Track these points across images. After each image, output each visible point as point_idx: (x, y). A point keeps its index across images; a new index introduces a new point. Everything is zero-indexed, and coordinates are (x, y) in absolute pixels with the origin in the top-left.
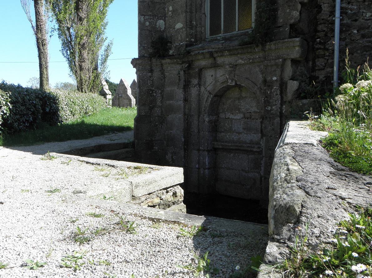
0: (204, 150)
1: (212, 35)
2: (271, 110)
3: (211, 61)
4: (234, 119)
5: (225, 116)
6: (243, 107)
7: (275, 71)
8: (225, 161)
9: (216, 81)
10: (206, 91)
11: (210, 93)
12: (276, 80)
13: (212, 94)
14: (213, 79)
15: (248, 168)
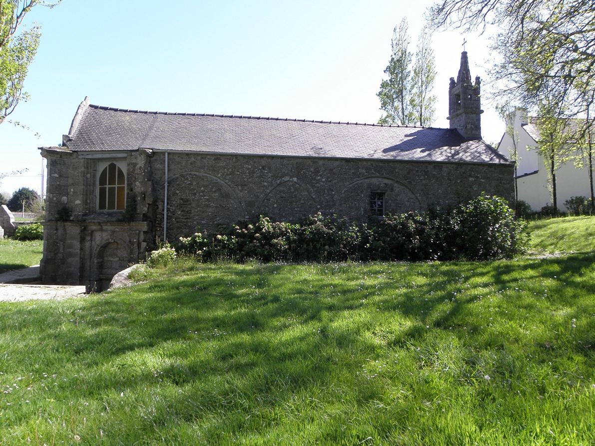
9: (102, 238)
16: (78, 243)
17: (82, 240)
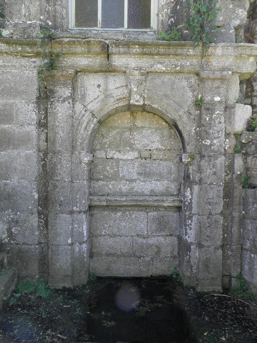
0: (80, 212)
1: (81, 26)
2: (211, 145)
3: (98, 61)
4: (122, 159)
5: (106, 155)
6: (138, 142)
7: (219, 87)
8: (106, 225)
9: (107, 96)
10: (86, 111)
11: (93, 115)
12: (220, 102)
13: (96, 118)
14: (98, 93)
15: (148, 231)
16: (32, 106)
17: (45, 97)
